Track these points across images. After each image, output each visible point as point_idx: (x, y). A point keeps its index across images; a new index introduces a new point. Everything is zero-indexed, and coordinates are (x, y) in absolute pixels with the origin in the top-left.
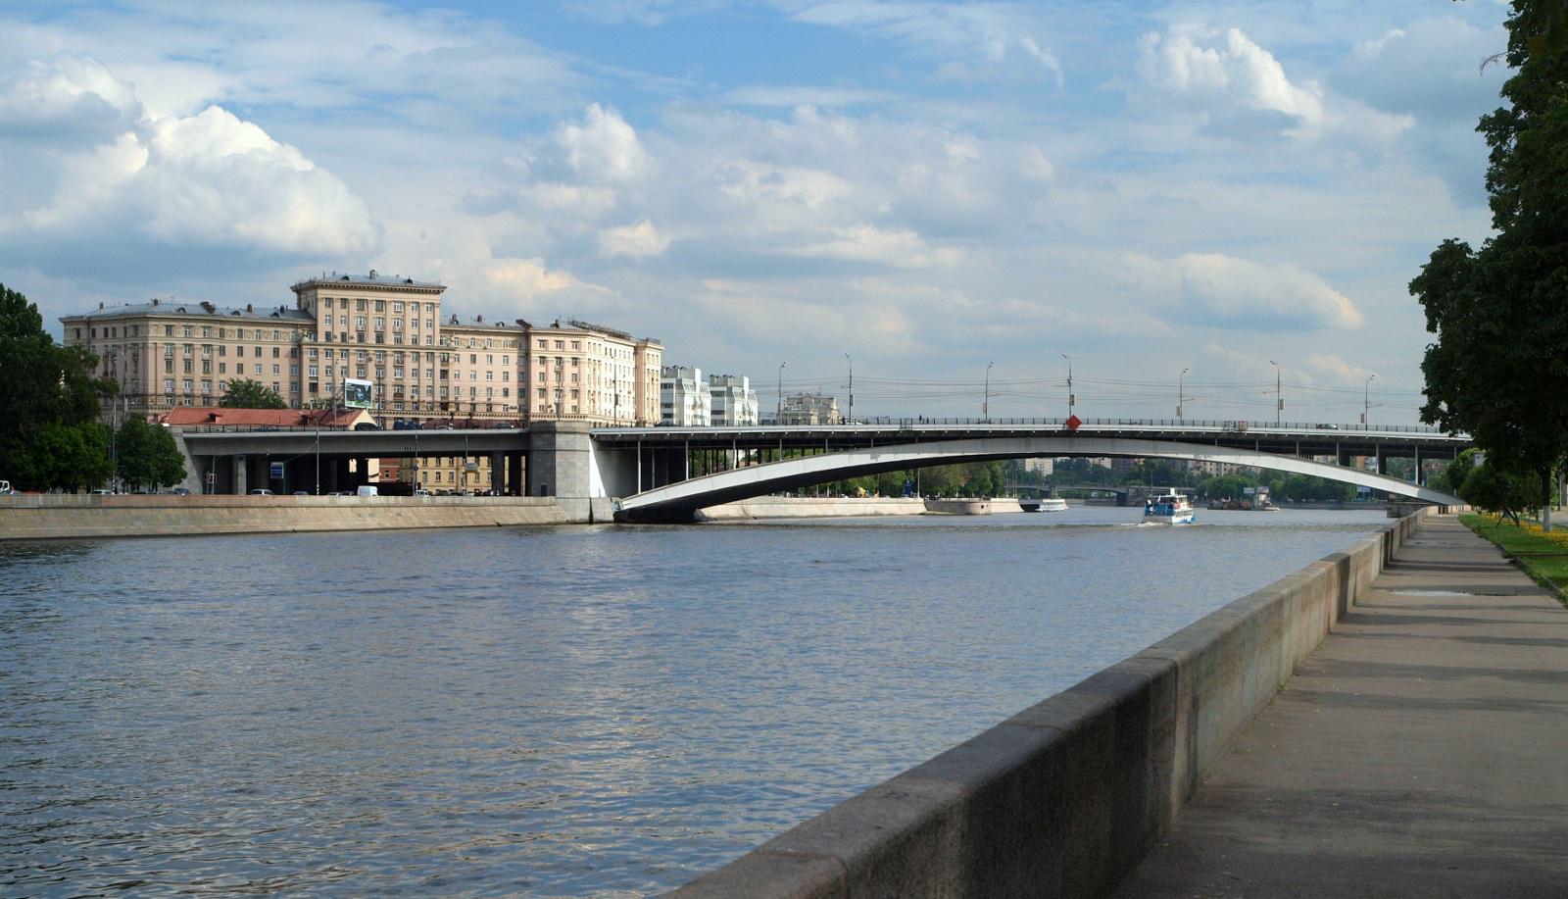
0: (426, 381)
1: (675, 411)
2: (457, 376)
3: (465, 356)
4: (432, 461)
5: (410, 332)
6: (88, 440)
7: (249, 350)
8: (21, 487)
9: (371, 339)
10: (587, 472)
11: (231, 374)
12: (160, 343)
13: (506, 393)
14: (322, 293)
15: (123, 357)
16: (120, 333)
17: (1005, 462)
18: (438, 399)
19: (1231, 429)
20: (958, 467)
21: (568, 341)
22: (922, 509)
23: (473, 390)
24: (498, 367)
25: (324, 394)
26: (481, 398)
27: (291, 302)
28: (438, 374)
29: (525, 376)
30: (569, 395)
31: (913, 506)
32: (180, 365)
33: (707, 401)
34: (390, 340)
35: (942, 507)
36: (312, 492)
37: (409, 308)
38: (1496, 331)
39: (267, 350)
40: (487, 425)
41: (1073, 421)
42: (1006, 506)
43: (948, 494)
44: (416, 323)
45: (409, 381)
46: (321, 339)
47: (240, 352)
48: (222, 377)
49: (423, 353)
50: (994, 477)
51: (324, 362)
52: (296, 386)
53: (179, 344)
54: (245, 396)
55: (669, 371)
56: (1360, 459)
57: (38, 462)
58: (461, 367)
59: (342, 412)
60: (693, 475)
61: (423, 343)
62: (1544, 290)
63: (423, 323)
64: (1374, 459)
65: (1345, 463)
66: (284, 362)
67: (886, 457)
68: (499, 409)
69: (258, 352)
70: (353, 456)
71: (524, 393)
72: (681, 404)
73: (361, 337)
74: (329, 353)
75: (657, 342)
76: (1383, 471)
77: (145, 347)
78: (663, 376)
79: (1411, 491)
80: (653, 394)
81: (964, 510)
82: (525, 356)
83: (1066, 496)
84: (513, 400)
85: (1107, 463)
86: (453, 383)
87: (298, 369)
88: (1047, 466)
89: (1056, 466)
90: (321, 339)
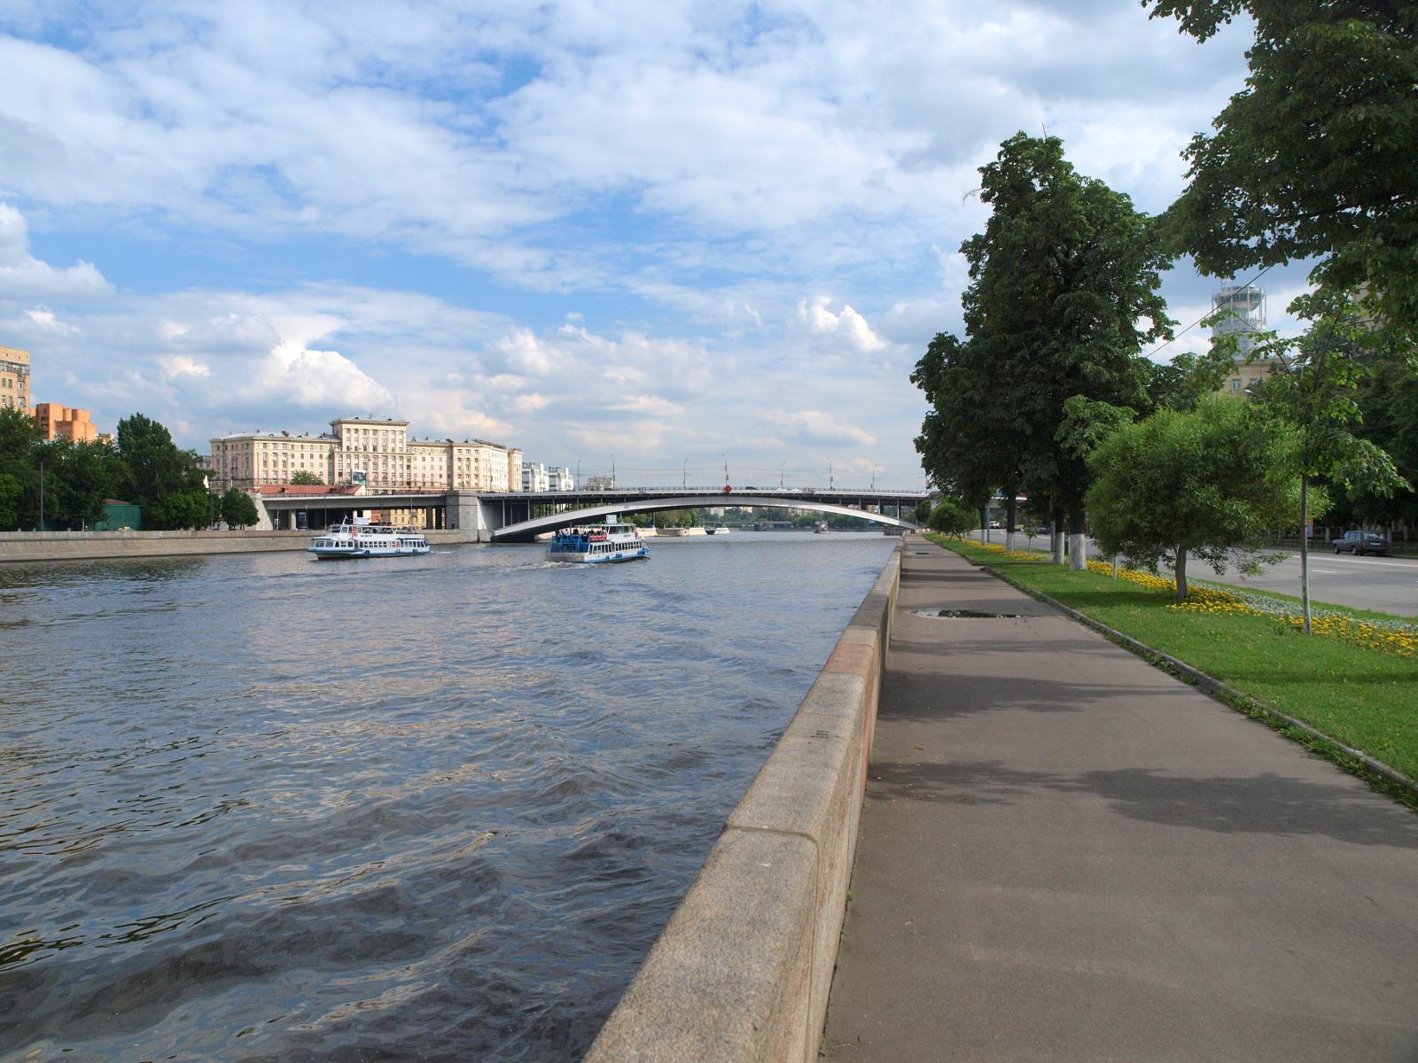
0: (399, 471)
1: (530, 485)
2: (415, 468)
3: (419, 458)
4: (399, 511)
5: (391, 446)
6: (196, 503)
7: (307, 455)
8: (173, 524)
9: (371, 450)
10: (476, 516)
11: (298, 468)
12: (260, 452)
13: (441, 476)
14: (344, 426)
15: (241, 460)
16: (240, 447)
17: (698, 510)
18: (405, 479)
19: (807, 492)
20: (674, 511)
21: (472, 449)
22: (655, 534)
23: (424, 475)
24: (437, 463)
25: (346, 477)
26: (428, 479)
27: (329, 430)
28: (405, 467)
29: (450, 468)
30: (473, 477)
31: (651, 532)
32: (271, 464)
33: (547, 480)
34: (380, 450)
35: (665, 532)
36: (39, 529)
37: (390, 433)
38: (977, 398)
39: (316, 456)
40: (430, 492)
41: (728, 488)
42: (698, 532)
43: (669, 526)
44: (394, 441)
45: (391, 471)
46: (345, 449)
47: (302, 456)
48: (293, 469)
49: (397, 456)
50: (693, 517)
51: (346, 461)
52: (331, 474)
53: (270, 453)
54: (303, 479)
55: (526, 465)
56: (870, 507)
57: (167, 513)
58: (417, 464)
59: (350, 487)
60: (532, 517)
61: (397, 451)
62: (1013, 366)
63: (397, 441)
64: (877, 507)
65: (864, 508)
66: (325, 462)
67: (632, 507)
68: (437, 485)
69: (312, 457)
70: (355, 509)
71: (450, 476)
72: (533, 482)
73: (365, 449)
74: (349, 457)
75: (519, 450)
76: (882, 512)
77: (252, 454)
78: (524, 467)
79: (895, 522)
80: (518, 477)
81: (676, 534)
82: (451, 458)
83: (730, 526)
84: (444, 480)
85: (750, 510)
86: (413, 471)
87: (331, 465)
88: (721, 512)
89: (725, 512)
90: (345, 449)
